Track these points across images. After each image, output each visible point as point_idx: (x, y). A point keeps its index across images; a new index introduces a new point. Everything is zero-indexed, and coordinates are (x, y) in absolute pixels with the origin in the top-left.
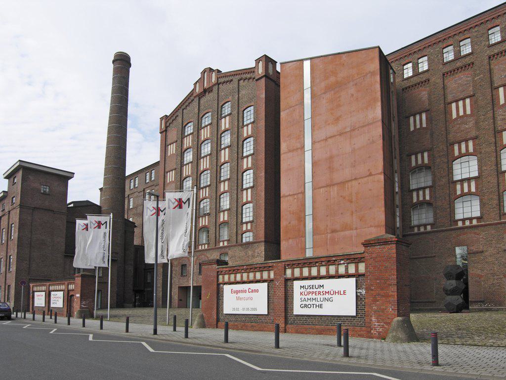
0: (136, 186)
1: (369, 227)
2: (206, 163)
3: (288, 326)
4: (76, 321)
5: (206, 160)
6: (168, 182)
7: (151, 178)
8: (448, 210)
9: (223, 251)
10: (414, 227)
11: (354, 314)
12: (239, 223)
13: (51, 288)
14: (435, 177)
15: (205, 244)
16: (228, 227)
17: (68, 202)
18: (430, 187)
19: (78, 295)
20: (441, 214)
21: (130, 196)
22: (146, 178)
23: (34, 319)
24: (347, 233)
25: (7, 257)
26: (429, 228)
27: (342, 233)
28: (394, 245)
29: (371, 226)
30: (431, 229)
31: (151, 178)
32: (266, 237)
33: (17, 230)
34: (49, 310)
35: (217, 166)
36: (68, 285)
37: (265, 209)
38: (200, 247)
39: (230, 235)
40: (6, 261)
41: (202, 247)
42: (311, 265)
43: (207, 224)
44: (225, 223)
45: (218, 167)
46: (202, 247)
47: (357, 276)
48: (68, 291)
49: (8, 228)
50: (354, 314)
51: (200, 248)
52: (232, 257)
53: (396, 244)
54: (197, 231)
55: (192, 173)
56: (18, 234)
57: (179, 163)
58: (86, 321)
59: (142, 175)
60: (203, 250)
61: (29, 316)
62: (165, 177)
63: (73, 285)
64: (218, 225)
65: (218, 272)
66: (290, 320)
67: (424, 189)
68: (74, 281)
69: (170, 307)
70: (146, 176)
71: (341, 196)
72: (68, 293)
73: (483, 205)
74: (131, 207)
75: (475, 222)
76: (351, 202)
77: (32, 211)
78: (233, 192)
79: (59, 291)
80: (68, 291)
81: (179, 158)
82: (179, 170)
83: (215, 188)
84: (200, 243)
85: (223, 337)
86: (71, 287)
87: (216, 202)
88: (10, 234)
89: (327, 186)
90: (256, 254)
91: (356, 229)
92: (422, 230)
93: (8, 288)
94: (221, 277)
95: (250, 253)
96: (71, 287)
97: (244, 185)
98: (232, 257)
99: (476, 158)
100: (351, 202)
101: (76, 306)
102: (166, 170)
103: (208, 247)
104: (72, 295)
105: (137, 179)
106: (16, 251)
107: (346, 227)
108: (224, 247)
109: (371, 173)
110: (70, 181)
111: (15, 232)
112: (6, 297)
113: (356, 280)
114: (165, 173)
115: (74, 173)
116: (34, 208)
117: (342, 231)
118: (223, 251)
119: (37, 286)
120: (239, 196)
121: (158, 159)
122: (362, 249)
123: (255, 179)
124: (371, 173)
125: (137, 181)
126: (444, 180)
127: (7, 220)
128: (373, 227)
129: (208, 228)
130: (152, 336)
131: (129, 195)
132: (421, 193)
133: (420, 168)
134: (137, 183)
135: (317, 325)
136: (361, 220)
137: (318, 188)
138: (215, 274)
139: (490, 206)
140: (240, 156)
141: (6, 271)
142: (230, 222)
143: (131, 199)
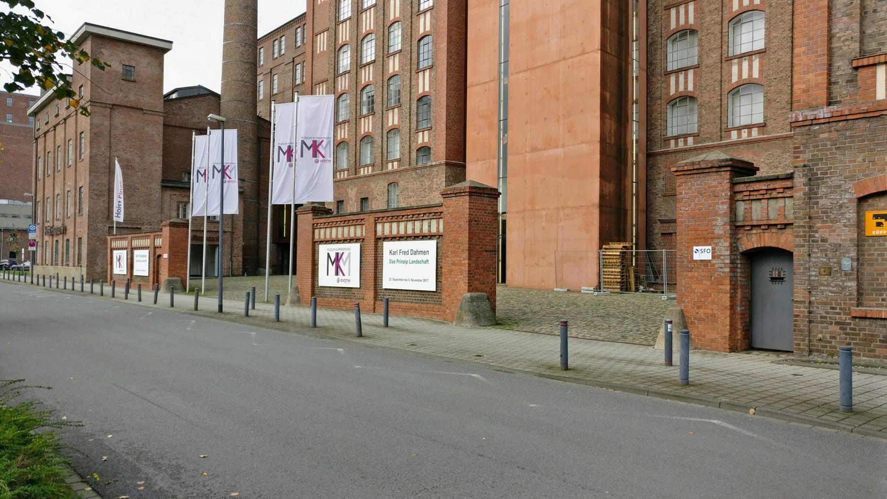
0: (283, 52)
1: (578, 144)
2: (370, 21)
3: (378, 302)
4: (164, 297)
5: (346, 25)
6: (318, 52)
7: (280, 50)
8: (718, 110)
9: (391, 178)
10: (669, 139)
11: (359, 287)
12: (413, 131)
13: (135, 243)
14: (702, 50)
15: (367, 166)
16: (372, 147)
17: (166, 91)
18: (760, 52)
19: (166, 256)
20: (707, 116)
21: (274, 72)
22: (296, 38)
23: (387, 324)
24: (552, 152)
25: (76, 189)
26: (690, 140)
27: (545, 153)
28: (467, 198)
29: (582, 143)
30: (694, 143)
31: (280, 50)
32: (448, 157)
33: (88, 144)
34: (130, 280)
35: (384, 26)
36: (132, 240)
37: (447, 106)
38: (390, 165)
39: (373, 157)
40: (75, 196)
41: (340, 175)
42: (399, 219)
43: (370, 131)
44: (394, 130)
45: (386, 28)
46: (340, 175)
47: (437, 236)
48: (155, 248)
49: (76, 140)
50: (359, 287)
51: (362, 173)
52: (404, 190)
53: (469, 195)
54: (358, 142)
55: (351, 38)
56: (90, 152)
57: (333, 18)
58: (176, 296)
59: (289, 32)
60: (365, 177)
61: (108, 289)
62: (313, 42)
63: (161, 239)
64: (385, 132)
65: (314, 224)
66: (317, 291)
67: (686, 69)
68: (161, 233)
69: (294, 273)
70: (296, 34)
71: (546, 89)
72: (155, 253)
73: (768, 102)
74: (275, 91)
75: (755, 133)
76: (558, 99)
77: (109, 110)
78: (406, 76)
79: (120, 249)
80: (155, 248)
81: (333, 9)
82: (333, 32)
83: (381, 66)
84: (363, 164)
85: (169, 301)
86: (159, 242)
87: (383, 91)
88: (78, 149)
89: (528, 69)
90: (435, 186)
91: (563, 146)
92: (681, 144)
93: (79, 241)
94: (379, 227)
95: (427, 183)
96: (159, 242)
97: (421, 63)
98: (404, 190)
99: (763, 15)
100: (558, 99)
101: (164, 276)
102: (316, 31)
103: (373, 170)
104: (160, 256)
105: (283, 38)
106: (88, 180)
107: (551, 143)
108: (394, 172)
109: (584, 49)
110: (167, 57)
111: (85, 148)
112: (76, 257)
113: (437, 243)
114: (315, 35)
115: (171, 42)
116: (113, 105)
117: (545, 149)
118: (391, 178)
119: (138, 238)
120: (413, 83)
121: (304, 10)
122: (442, 200)
123: (435, 56)
124: (584, 49)
125: (283, 43)
126: (715, 56)
127: (74, 126)
128: (584, 143)
129: (372, 138)
130: (152, 306)
131: (271, 69)
132: (745, 65)
133: (686, 32)
134: (283, 47)
135: (403, 302)
136: (569, 131)
137: (516, 73)
138: (311, 229)
139: (778, 105)
140: (415, 10)
141: (75, 213)
142: (401, 128)
143: (276, 77)
